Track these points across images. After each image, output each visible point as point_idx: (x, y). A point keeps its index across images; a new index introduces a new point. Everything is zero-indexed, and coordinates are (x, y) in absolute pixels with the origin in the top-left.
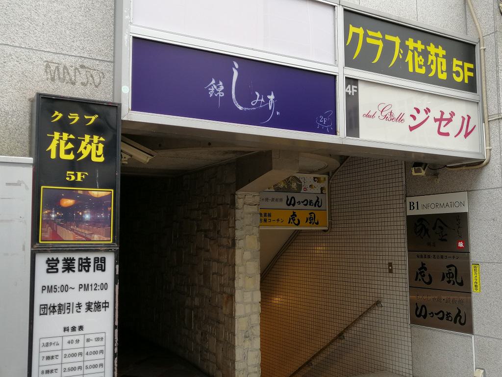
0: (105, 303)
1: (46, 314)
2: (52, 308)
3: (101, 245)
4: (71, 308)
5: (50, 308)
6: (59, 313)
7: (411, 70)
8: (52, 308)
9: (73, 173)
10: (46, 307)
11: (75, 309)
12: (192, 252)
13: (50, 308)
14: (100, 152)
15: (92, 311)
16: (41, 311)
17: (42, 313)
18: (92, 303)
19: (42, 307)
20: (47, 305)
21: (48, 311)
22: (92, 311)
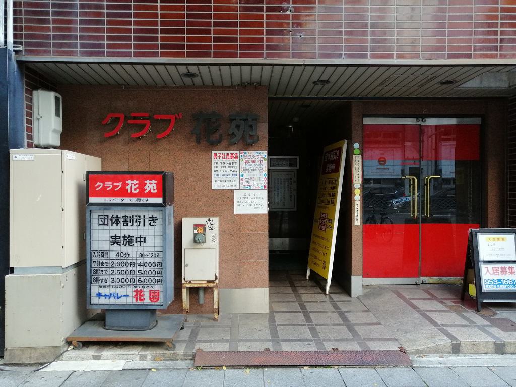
0: (140, 237)
1: (107, 225)
2: (114, 220)
3: (423, 202)
4: (142, 221)
5: (111, 219)
6: (124, 225)
7: (129, 191)
8: (114, 220)
9: (111, 183)
10: (106, 217)
11: (147, 222)
12: (443, 129)
13: (111, 219)
14: (155, 188)
15: (120, 245)
16: (100, 221)
17: (101, 223)
18: (120, 237)
19: (100, 217)
20: (107, 216)
21: (110, 222)
22: (120, 245)
